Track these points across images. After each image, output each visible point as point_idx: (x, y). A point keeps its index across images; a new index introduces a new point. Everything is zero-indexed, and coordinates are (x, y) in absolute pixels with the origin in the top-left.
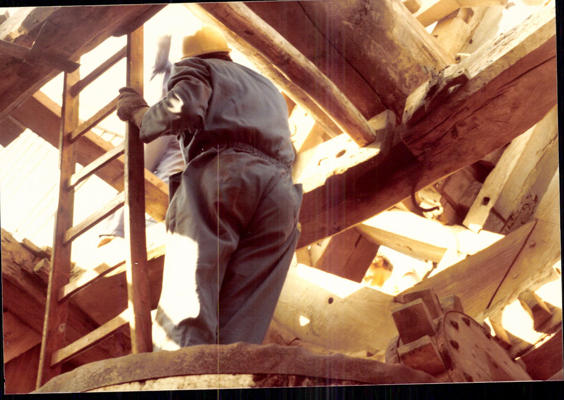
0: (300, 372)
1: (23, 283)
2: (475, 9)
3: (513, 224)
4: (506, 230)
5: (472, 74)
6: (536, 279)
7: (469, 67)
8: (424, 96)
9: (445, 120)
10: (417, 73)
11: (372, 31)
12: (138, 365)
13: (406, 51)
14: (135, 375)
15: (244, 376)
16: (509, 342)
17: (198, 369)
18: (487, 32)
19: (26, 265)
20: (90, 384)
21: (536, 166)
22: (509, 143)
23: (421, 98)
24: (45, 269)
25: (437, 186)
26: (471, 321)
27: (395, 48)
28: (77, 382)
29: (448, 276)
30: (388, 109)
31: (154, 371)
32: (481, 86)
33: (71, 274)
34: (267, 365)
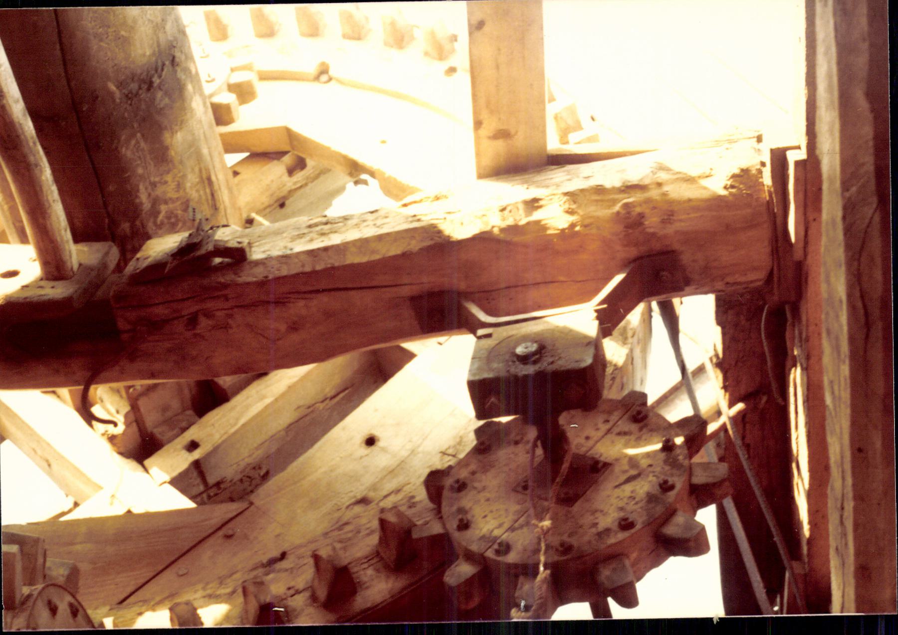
2: (310, 163)
3: (216, 495)
4: (203, 498)
5: (256, 254)
6: (209, 592)
7: (256, 242)
8: (172, 250)
9: (188, 299)
10: (179, 212)
11: (144, 120)
13: (180, 172)
18: (312, 203)
21: (287, 427)
22: (265, 374)
23: (167, 251)
25: (131, 390)
26: (81, 612)
27: (167, 160)
29: (83, 529)
30: (114, 241)
32: (260, 277)
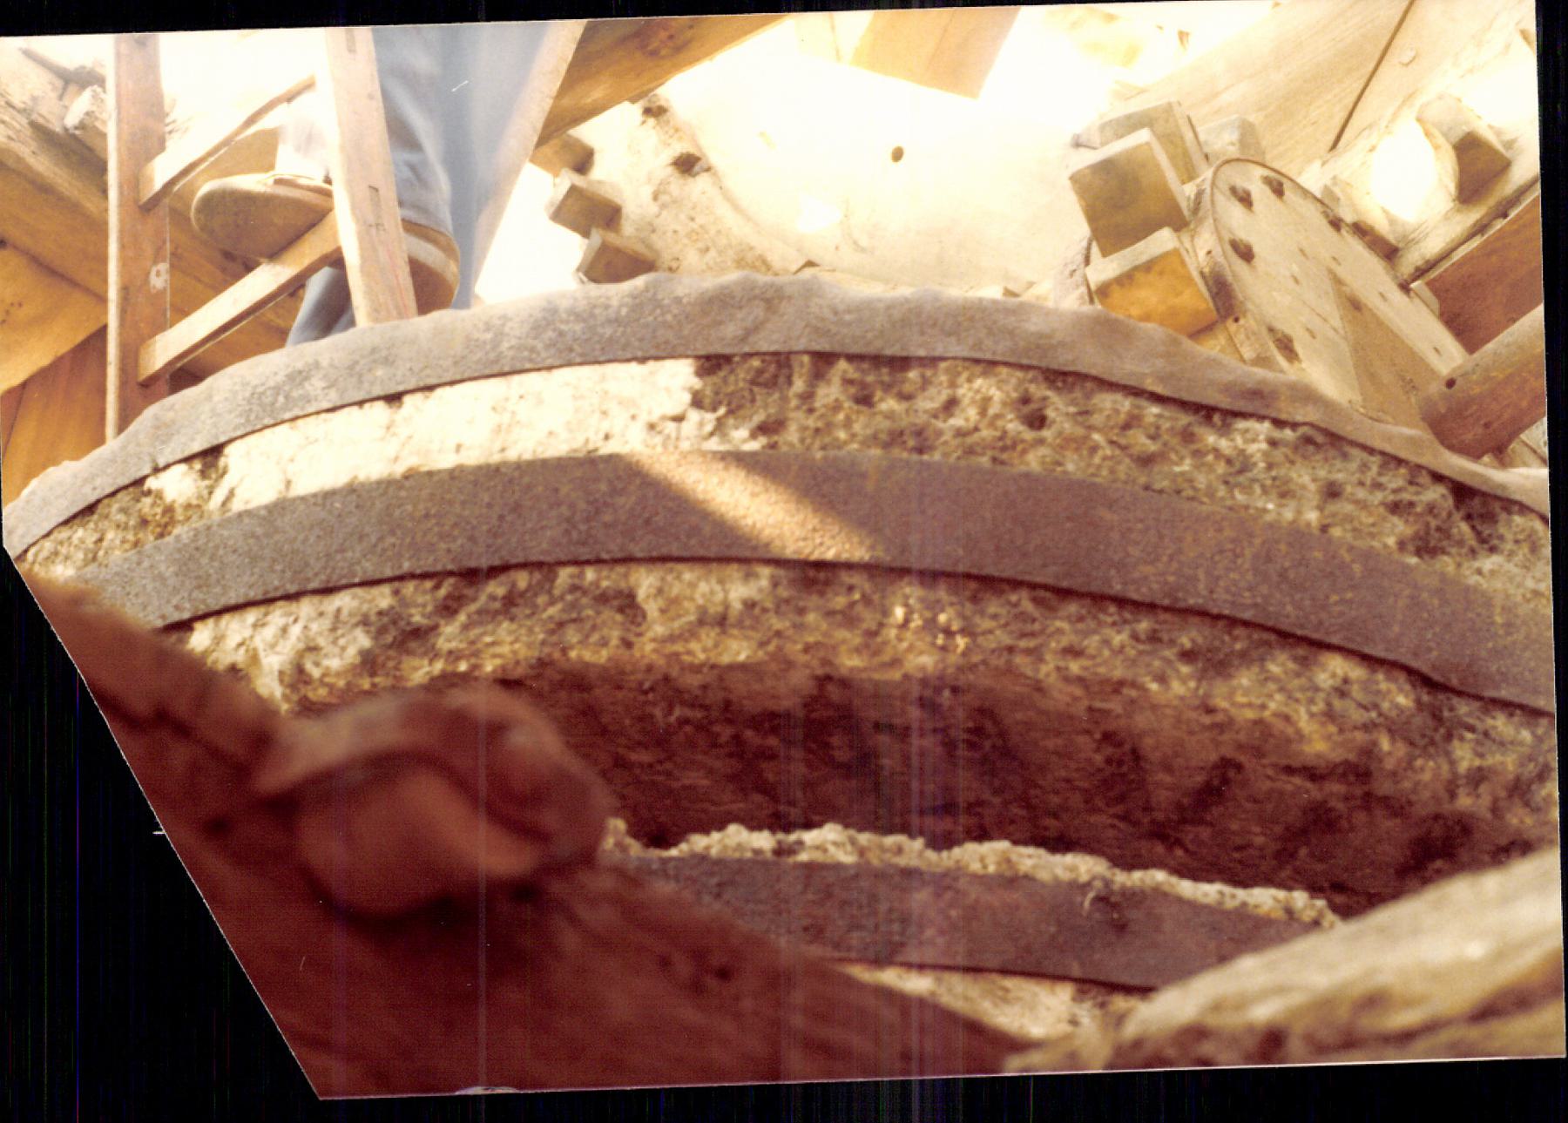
0: (823, 345)
1: (42, 164)
12: (377, 356)
14: (372, 384)
15: (669, 365)
16: (1391, 238)
17: (544, 355)
19: (43, 110)
20: (252, 417)
24: (97, 118)
26: (1287, 186)
28: (214, 413)
31: (421, 370)
33: (168, 129)
34: (731, 330)
